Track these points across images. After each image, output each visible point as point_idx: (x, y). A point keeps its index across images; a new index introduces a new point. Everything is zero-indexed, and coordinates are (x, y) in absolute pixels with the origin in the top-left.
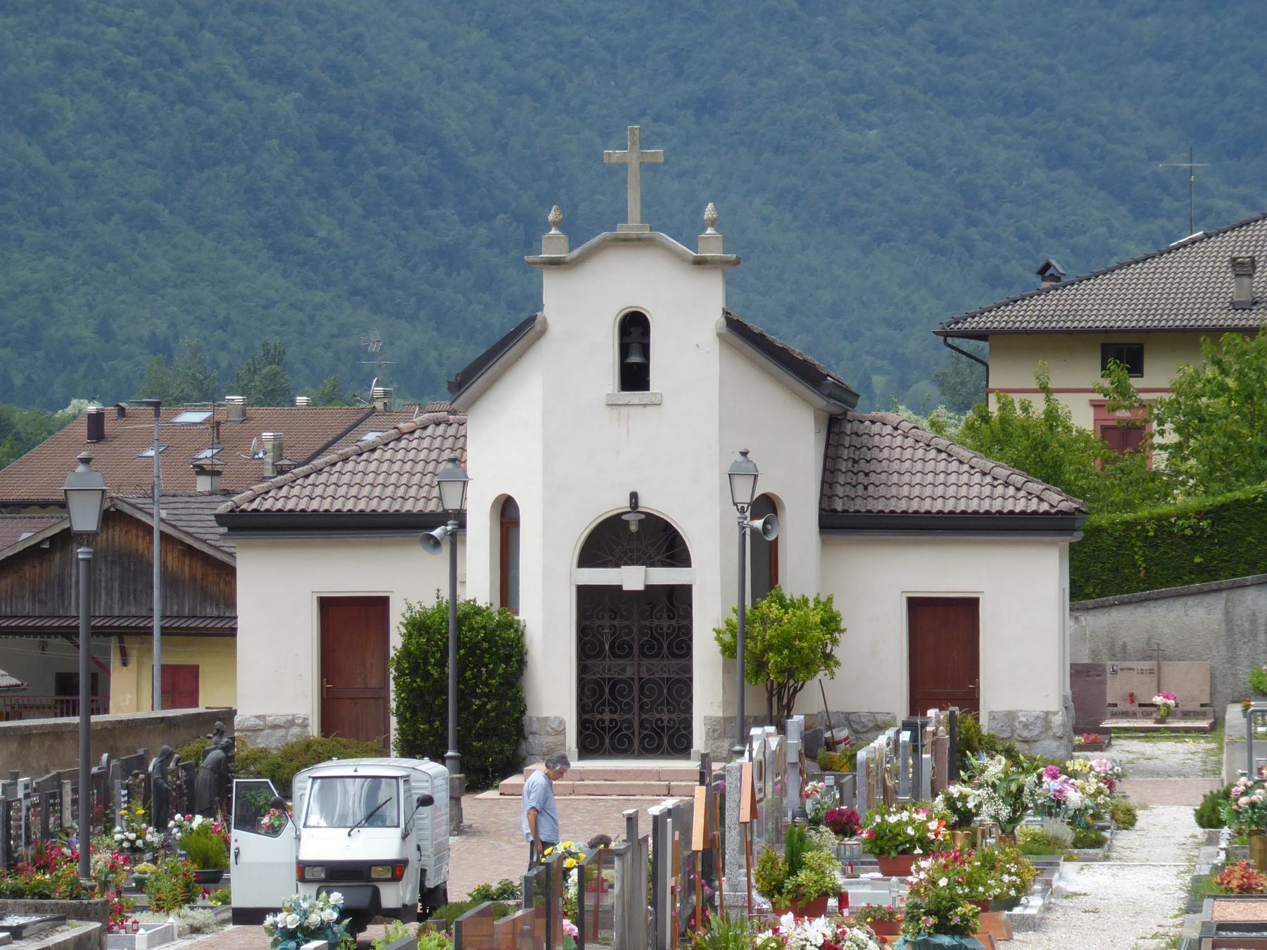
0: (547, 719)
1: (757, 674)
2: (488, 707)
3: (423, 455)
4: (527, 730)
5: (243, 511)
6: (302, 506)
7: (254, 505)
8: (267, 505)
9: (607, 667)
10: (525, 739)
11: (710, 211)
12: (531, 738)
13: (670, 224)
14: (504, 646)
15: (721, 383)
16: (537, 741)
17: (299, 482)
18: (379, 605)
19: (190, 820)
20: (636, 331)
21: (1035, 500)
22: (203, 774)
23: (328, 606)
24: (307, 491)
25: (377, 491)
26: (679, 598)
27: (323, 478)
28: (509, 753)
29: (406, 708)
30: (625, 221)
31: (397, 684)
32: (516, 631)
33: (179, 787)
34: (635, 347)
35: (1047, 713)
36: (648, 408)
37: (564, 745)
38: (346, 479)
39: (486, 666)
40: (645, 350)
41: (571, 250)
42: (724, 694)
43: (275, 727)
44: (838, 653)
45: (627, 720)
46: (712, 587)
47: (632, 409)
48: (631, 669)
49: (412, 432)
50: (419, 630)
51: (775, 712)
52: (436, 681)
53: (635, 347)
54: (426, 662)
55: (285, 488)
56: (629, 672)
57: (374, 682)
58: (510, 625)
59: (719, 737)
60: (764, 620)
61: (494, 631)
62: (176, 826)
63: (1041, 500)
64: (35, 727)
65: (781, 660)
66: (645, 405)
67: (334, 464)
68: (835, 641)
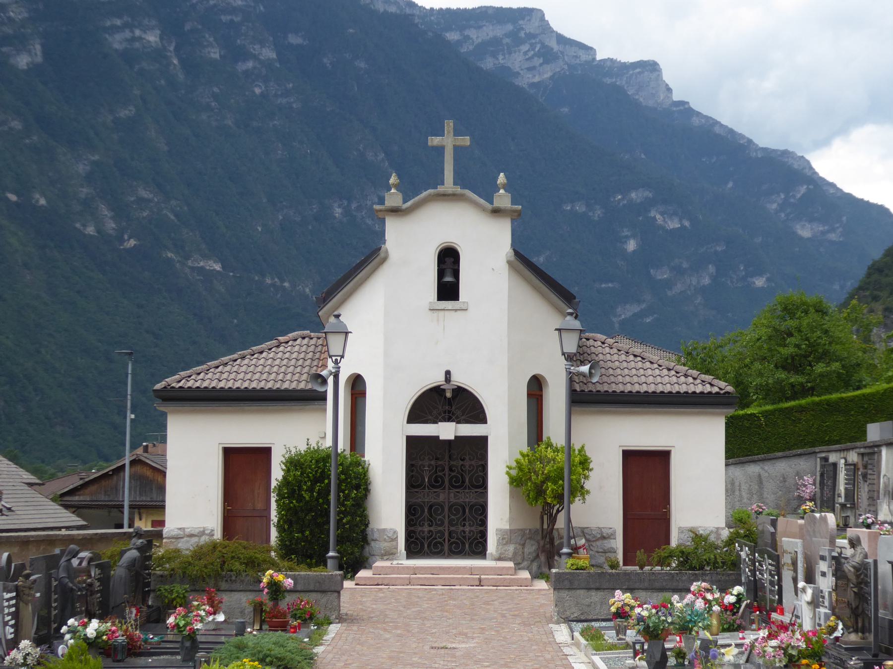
0: (384, 530)
1: (536, 499)
2: (344, 521)
3: (295, 355)
4: (369, 538)
5: (173, 387)
6: (213, 384)
7: (180, 384)
8: (189, 384)
9: (426, 497)
10: (368, 544)
11: (502, 178)
12: (373, 544)
13: (475, 183)
14: (356, 478)
15: (509, 296)
16: (378, 546)
17: (212, 370)
18: (264, 453)
19: (85, 625)
20: (449, 260)
21: (708, 385)
22: (119, 572)
23: (231, 455)
24: (217, 376)
25: (265, 376)
26: (482, 441)
27: (228, 368)
28: (357, 554)
29: (285, 522)
30: (443, 184)
31: (278, 505)
32: (363, 468)
33: (91, 585)
34: (449, 272)
35: (718, 528)
36: (459, 312)
37: (397, 548)
38: (244, 369)
39: (343, 491)
40: (456, 274)
41: (405, 201)
42: (510, 512)
43: (191, 536)
44: (587, 486)
45: (439, 532)
46: (503, 441)
47: (447, 313)
48: (443, 497)
49: (287, 342)
50: (296, 466)
51: (545, 526)
52: (307, 502)
53: (449, 272)
54: (300, 488)
55: (202, 374)
56: (442, 497)
57: (260, 506)
58: (358, 464)
59: (506, 544)
60: (541, 460)
61: (348, 467)
62: (68, 632)
63: (712, 385)
64: (32, 536)
65: (549, 486)
66: (456, 310)
67: (235, 360)
68: (586, 477)
